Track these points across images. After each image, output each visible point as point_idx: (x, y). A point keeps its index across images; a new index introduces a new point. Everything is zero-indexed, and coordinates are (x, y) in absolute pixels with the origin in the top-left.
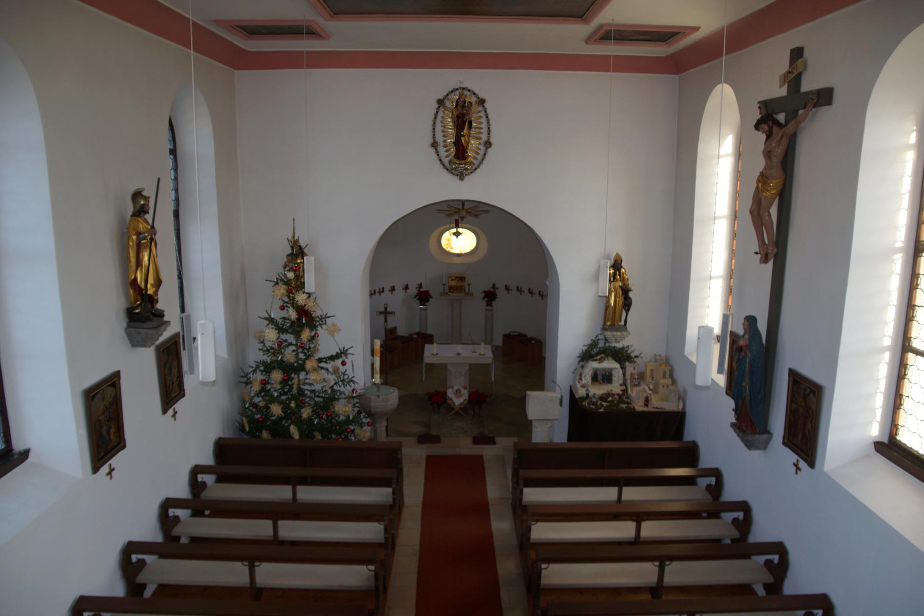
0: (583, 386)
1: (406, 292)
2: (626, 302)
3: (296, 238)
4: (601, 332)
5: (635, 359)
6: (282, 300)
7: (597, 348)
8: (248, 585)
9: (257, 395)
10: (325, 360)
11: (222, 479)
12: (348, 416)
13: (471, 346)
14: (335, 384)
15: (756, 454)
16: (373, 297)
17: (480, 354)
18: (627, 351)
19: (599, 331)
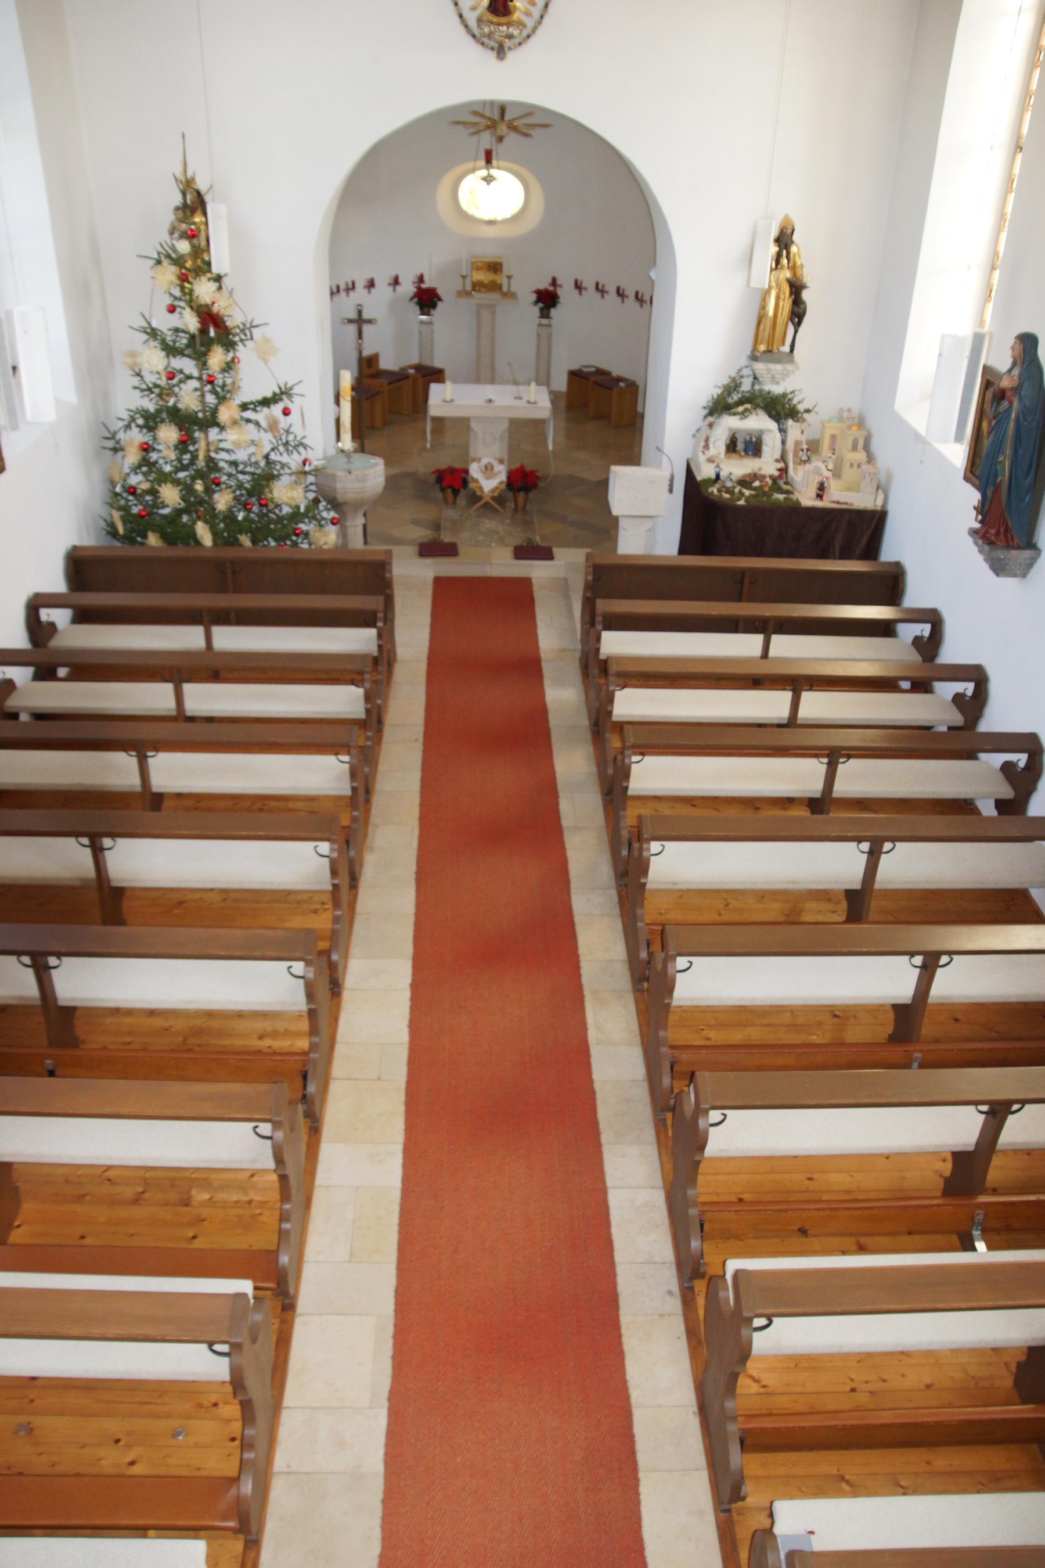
0: (710, 460)
1: (394, 290)
2: (796, 309)
3: (190, 174)
4: (748, 364)
5: (805, 416)
6: (171, 294)
7: (738, 393)
8: (139, 789)
9: (136, 469)
10: (252, 406)
11: (84, 616)
12: (298, 507)
13: (514, 388)
14: (273, 449)
15: (1008, 583)
16: (336, 298)
17: (529, 402)
18: (790, 400)
19: (744, 361)
